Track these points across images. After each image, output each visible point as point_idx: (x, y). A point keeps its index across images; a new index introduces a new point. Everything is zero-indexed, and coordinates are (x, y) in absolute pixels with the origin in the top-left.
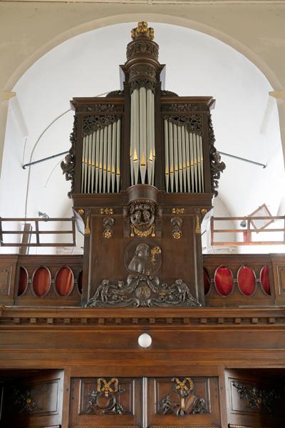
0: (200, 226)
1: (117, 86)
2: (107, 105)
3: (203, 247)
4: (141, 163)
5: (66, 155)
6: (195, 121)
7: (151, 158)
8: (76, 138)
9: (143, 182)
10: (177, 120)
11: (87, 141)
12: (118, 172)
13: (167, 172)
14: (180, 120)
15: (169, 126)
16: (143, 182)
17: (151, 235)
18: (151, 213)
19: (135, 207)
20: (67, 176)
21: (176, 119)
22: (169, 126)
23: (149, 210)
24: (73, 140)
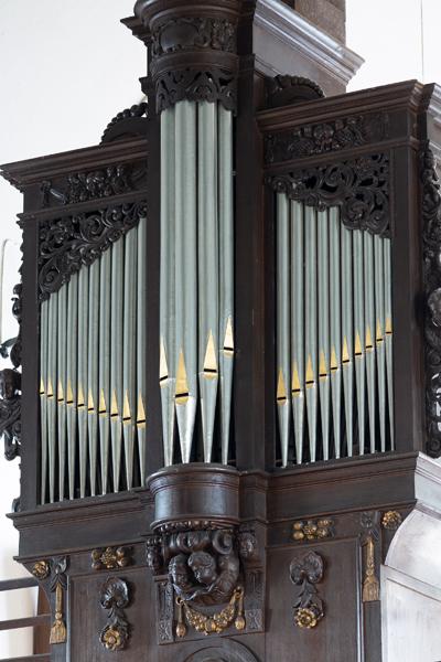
0: (377, 574)
1: (137, 96)
2: (104, 171)
3: (390, 335)
4: (139, 419)
5: (343, 226)
6: (368, 182)
7: (210, 361)
8: (27, 305)
9: (186, 458)
10: (315, 191)
11: (52, 311)
12: (141, 415)
13: (282, 390)
14: (325, 187)
15: (307, 208)
16: (186, 458)
17: (231, 623)
18: (217, 556)
19: (168, 543)
20: (8, 442)
21: (311, 183)
22: (289, 213)
23: (209, 549)
24: (18, 310)
